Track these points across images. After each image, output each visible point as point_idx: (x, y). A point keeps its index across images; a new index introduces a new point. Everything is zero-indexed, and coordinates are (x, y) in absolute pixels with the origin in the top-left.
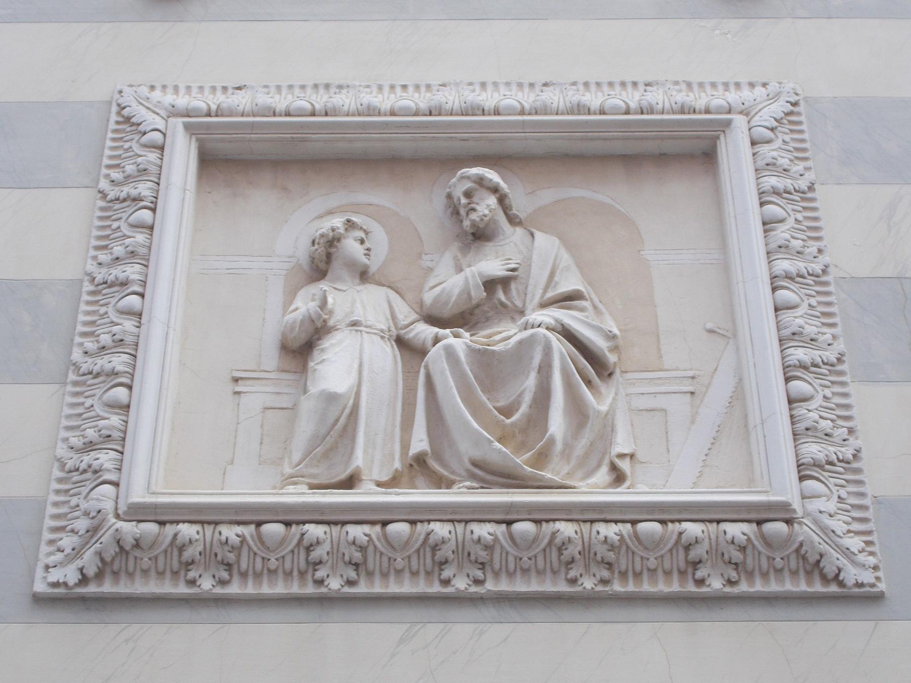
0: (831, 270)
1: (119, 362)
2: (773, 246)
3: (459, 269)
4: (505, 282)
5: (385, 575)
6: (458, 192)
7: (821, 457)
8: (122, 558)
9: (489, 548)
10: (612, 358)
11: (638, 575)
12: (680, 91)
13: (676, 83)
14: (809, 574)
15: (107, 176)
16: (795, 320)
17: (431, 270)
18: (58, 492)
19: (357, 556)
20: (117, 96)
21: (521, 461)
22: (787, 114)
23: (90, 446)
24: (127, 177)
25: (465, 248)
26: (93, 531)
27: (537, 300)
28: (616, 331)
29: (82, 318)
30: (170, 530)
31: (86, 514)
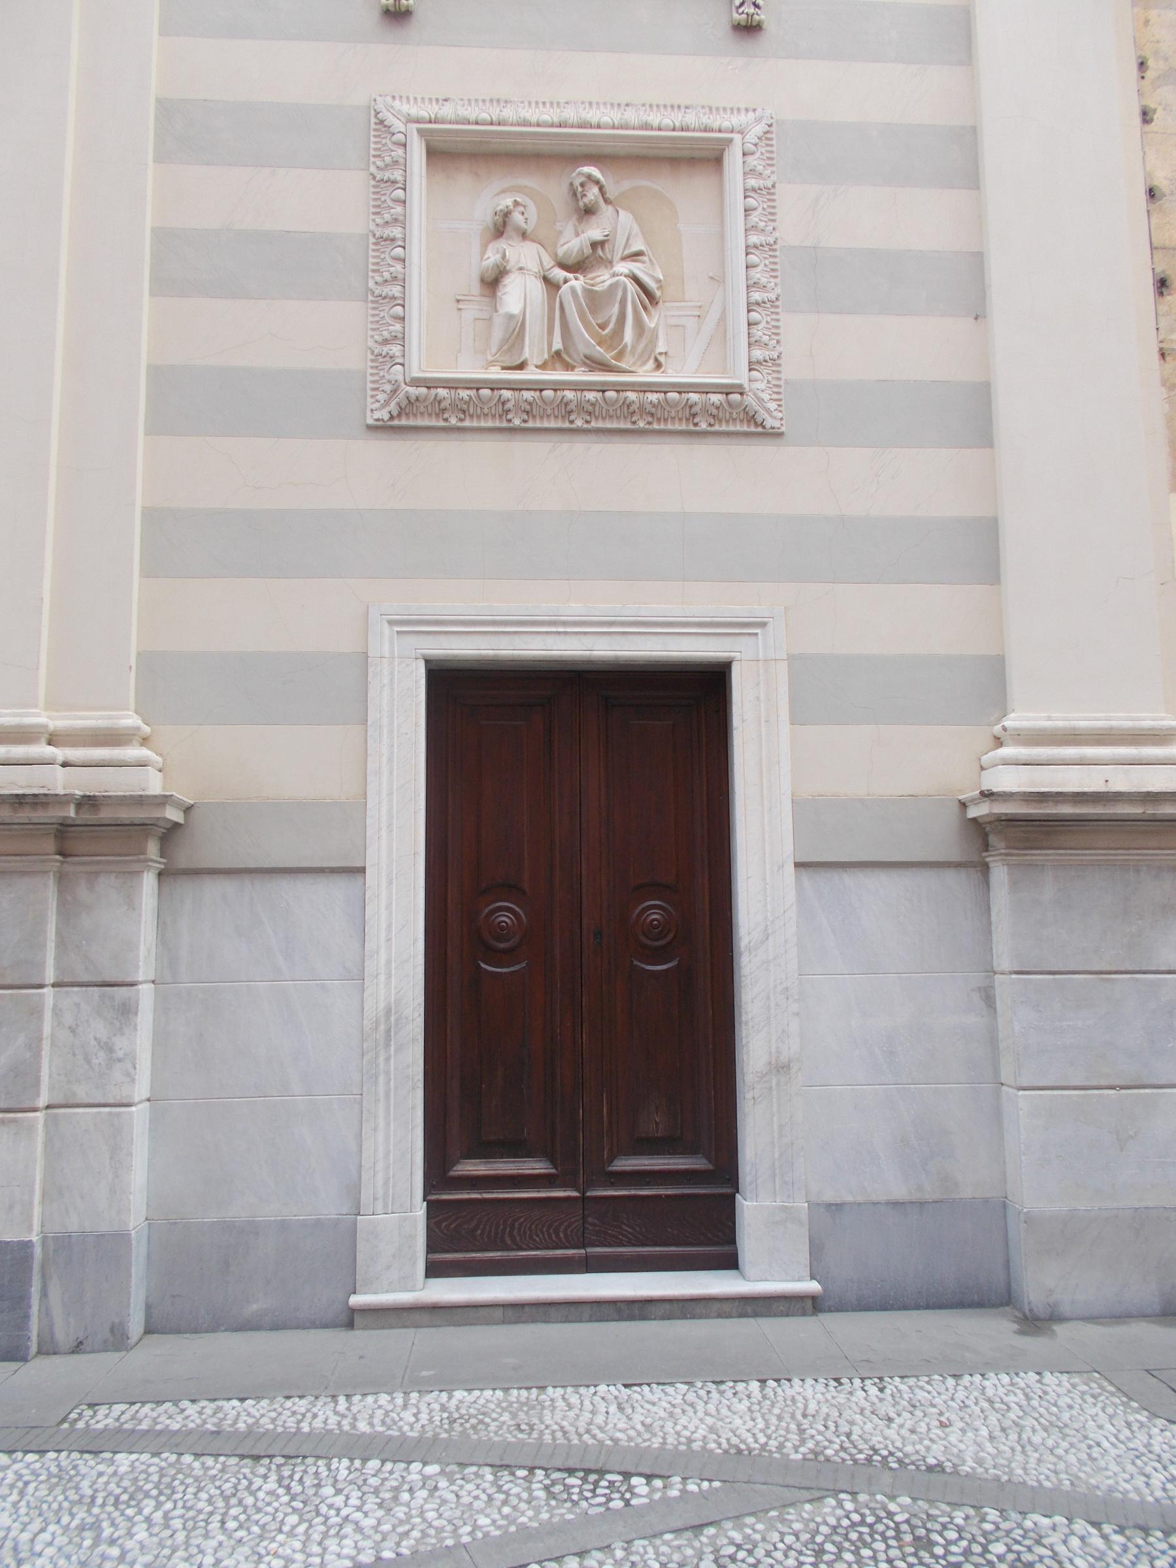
0: (779, 241)
1: (396, 290)
2: (749, 226)
3: (577, 235)
4: (602, 243)
5: (542, 418)
6: (577, 183)
7: (756, 186)
8: (410, 406)
9: (593, 405)
10: (658, 293)
11: (666, 420)
12: (705, 114)
13: (703, 107)
14: (749, 421)
15: (374, 163)
16: (756, 274)
17: (560, 232)
18: (372, 367)
19: (528, 408)
20: (373, 103)
21: (609, 357)
22: (766, 133)
23: (386, 342)
24: (387, 166)
25: (580, 220)
26: (394, 391)
27: (619, 256)
28: (661, 277)
29: (371, 260)
30: (433, 391)
31: (389, 382)
